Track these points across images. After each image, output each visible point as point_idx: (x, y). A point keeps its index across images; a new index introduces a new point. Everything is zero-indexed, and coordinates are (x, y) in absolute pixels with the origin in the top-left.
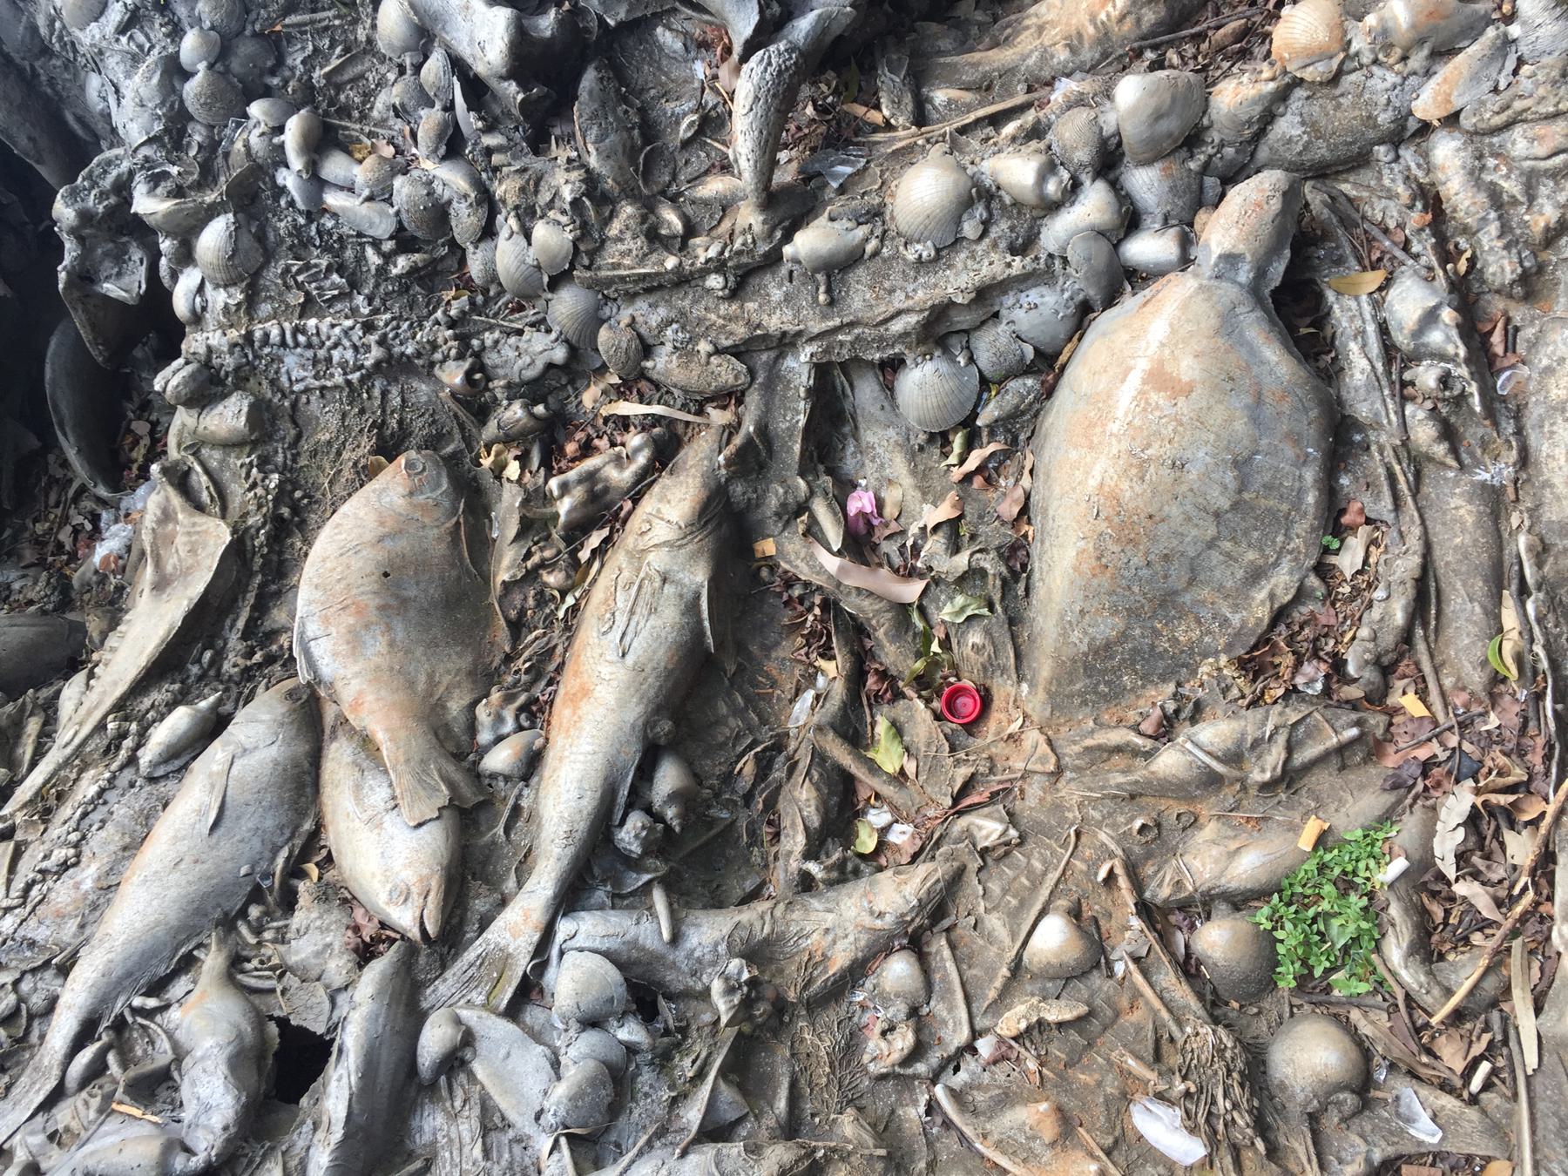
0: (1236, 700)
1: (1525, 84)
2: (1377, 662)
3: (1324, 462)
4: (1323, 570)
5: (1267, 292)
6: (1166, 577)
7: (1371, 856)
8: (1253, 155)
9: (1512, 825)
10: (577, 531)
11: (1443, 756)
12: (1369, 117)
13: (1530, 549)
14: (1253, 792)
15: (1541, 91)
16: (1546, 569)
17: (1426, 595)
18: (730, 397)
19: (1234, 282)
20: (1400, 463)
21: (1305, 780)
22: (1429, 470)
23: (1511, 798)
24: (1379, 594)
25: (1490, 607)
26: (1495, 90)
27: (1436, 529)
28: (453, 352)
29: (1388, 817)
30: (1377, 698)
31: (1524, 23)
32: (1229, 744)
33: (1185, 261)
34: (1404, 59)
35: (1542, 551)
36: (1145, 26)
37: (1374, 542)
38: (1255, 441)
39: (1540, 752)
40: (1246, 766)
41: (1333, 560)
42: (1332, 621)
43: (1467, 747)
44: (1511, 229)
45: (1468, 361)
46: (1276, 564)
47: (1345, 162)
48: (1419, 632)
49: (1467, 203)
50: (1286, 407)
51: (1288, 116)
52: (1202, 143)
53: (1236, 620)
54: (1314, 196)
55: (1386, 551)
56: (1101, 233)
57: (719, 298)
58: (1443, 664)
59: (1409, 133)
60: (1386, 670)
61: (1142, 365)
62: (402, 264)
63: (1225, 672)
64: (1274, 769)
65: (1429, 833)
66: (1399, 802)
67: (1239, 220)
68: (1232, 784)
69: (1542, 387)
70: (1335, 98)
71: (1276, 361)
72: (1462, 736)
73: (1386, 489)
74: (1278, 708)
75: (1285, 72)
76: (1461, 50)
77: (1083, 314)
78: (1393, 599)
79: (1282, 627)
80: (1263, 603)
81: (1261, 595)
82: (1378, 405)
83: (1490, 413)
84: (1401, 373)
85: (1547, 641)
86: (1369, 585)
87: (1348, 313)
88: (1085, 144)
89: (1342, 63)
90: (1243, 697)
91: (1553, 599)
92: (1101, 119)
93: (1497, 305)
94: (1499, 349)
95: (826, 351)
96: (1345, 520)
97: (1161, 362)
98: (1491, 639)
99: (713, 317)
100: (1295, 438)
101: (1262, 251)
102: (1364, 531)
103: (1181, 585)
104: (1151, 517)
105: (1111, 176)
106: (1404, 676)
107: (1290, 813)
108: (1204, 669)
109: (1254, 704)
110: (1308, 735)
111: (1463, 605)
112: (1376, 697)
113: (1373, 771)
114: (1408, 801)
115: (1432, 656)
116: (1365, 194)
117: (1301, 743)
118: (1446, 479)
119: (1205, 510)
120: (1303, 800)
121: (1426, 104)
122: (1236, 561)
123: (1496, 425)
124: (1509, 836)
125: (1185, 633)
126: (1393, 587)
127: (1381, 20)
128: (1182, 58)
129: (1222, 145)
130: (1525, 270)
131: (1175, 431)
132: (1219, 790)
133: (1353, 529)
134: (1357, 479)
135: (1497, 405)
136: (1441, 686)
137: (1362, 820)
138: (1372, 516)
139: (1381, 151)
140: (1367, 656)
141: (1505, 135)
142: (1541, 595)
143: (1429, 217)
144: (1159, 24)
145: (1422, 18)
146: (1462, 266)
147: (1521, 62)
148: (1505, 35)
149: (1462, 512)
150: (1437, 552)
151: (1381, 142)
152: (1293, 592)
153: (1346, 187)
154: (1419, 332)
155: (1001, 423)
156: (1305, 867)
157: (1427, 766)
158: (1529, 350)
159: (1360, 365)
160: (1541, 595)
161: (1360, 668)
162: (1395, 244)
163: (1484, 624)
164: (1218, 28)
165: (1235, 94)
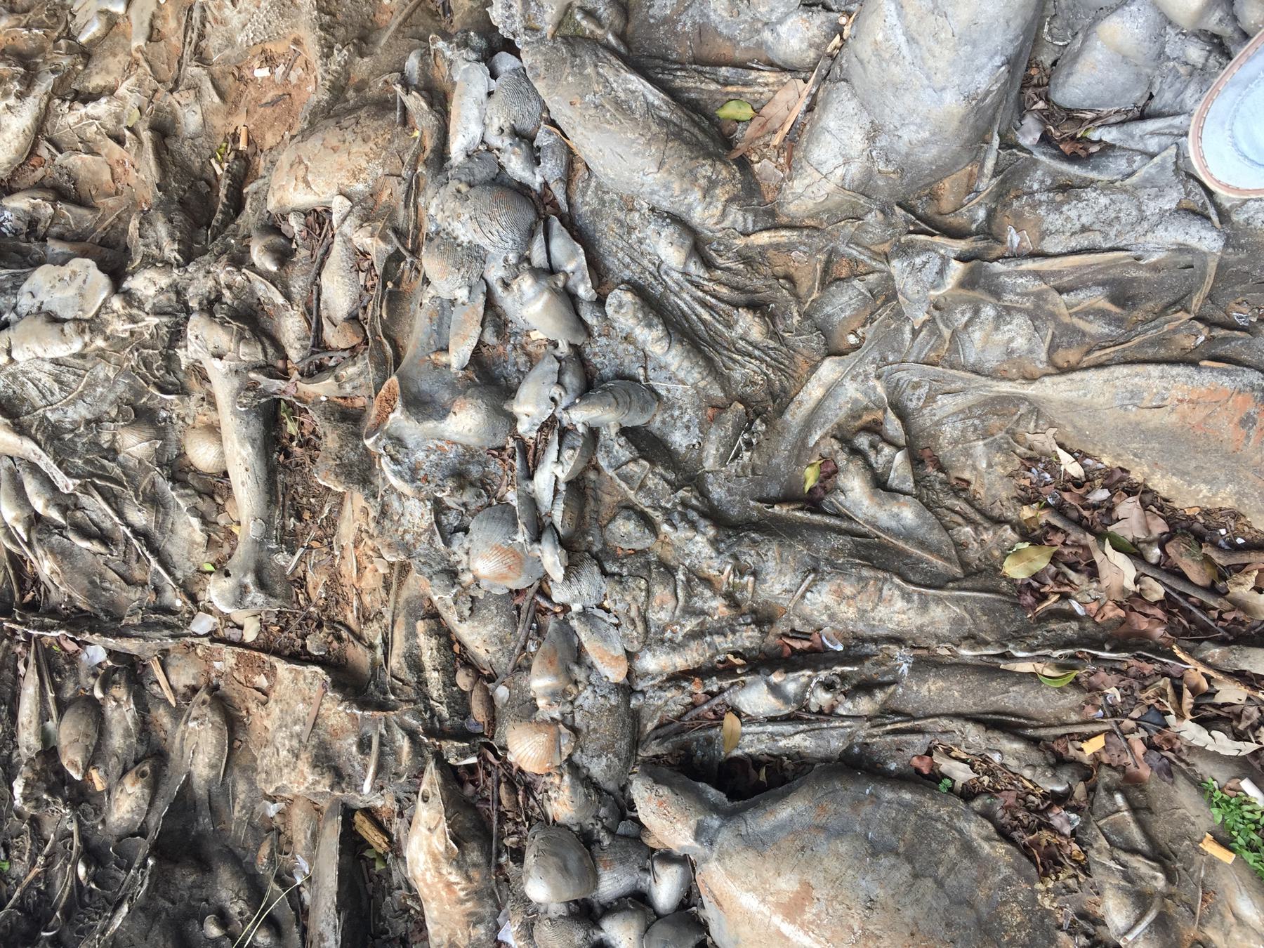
0: (1079, 883)
1: (620, 607)
2: (1054, 767)
3: (879, 782)
4: (968, 794)
5: (729, 804)
6: (965, 928)
7: (1239, 806)
8: (609, 793)
9: (1212, 694)
11: (1144, 734)
12: (610, 710)
13: (972, 648)
14: (1174, 889)
15: (628, 598)
16: (989, 639)
19: (718, 830)
20: (885, 725)
21: (1162, 842)
22: (893, 705)
23: (1187, 693)
24: (996, 758)
25: (1014, 680)
26: (617, 626)
27: (943, 707)
29: (1199, 784)
30: (1086, 772)
31: (574, 601)
32: (1128, 902)
33: (684, 861)
34: (576, 683)
35: (974, 640)
36: (481, 860)
37: (947, 752)
38: (857, 836)
39: (1144, 664)
40: (1148, 890)
41: (959, 785)
42: (1013, 794)
43: (1136, 714)
44: (722, 628)
45: (816, 670)
46: (960, 832)
47: (634, 728)
48: (1030, 732)
49: (695, 655)
50: (832, 807)
51: (591, 767)
52: (590, 833)
53: (1006, 871)
54: (653, 749)
55: (958, 746)
56: (647, 930)
58: (1059, 719)
60: (1060, 762)
61: (777, 920)
63: (1050, 886)
64: (1153, 868)
65: (1215, 757)
66: (1183, 772)
67: (665, 818)
68: (1166, 906)
69: (843, 622)
70: (588, 733)
71: (789, 810)
72: (1126, 716)
73: (904, 738)
74: (1092, 853)
75: (560, 766)
76: (580, 644)
78: (1002, 749)
79: (1015, 835)
80: (993, 847)
81: (986, 848)
82: (834, 733)
83: (859, 659)
84: (810, 712)
85: (1049, 646)
86: (985, 761)
87: (753, 742)
88: (570, 932)
89: (566, 726)
90: (1076, 877)
91: (1014, 638)
92: (553, 915)
93: (772, 640)
94: (807, 644)
96: (926, 771)
97: (778, 905)
98: (1041, 682)
100: (857, 803)
101: (699, 806)
102: (937, 758)
103: (971, 914)
104: (912, 935)
105: (599, 911)
106: (1067, 749)
107: (1198, 864)
108: (1047, 903)
109: (1086, 869)
110: (1119, 833)
111: (1011, 698)
112: (1083, 772)
113: (1153, 786)
114: (1183, 766)
115: (1051, 726)
116: (659, 714)
117: (1127, 840)
118: (904, 695)
119: (911, 886)
120: (1182, 849)
122: (955, 865)
123: (867, 656)
124: (1219, 699)
126: (991, 747)
127: (544, 696)
128: (514, 833)
129: (597, 817)
130: (753, 622)
131: (841, 903)
132: (1171, 917)
133: (933, 766)
134: (892, 757)
135: (851, 653)
136: (1078, 723)
137: (1202, 806)
138: (925, 750)
139: (634, 703)
140: (1049, 774)
141: (651, 623)
142: (1011, 645)
143: (697, 680)
144: (482, 849)
145: (552, 669)
146: (739, 661)
147: (600, 606)
148: (579, 614)
149: (933, 688)
150: (964, 710)
151: (629, 702)
152: (985, 822)
153: (650, 727)
154: (785, 698)
156: (1251, 862)
157: (1150, 746)
158: (811, 625)
159: (799, 740)
160: (1011, 645)
161: (1059, 782)
162: (707, 702)
163: (1029, 686)
164: (500, 802)
165: (563, 804)
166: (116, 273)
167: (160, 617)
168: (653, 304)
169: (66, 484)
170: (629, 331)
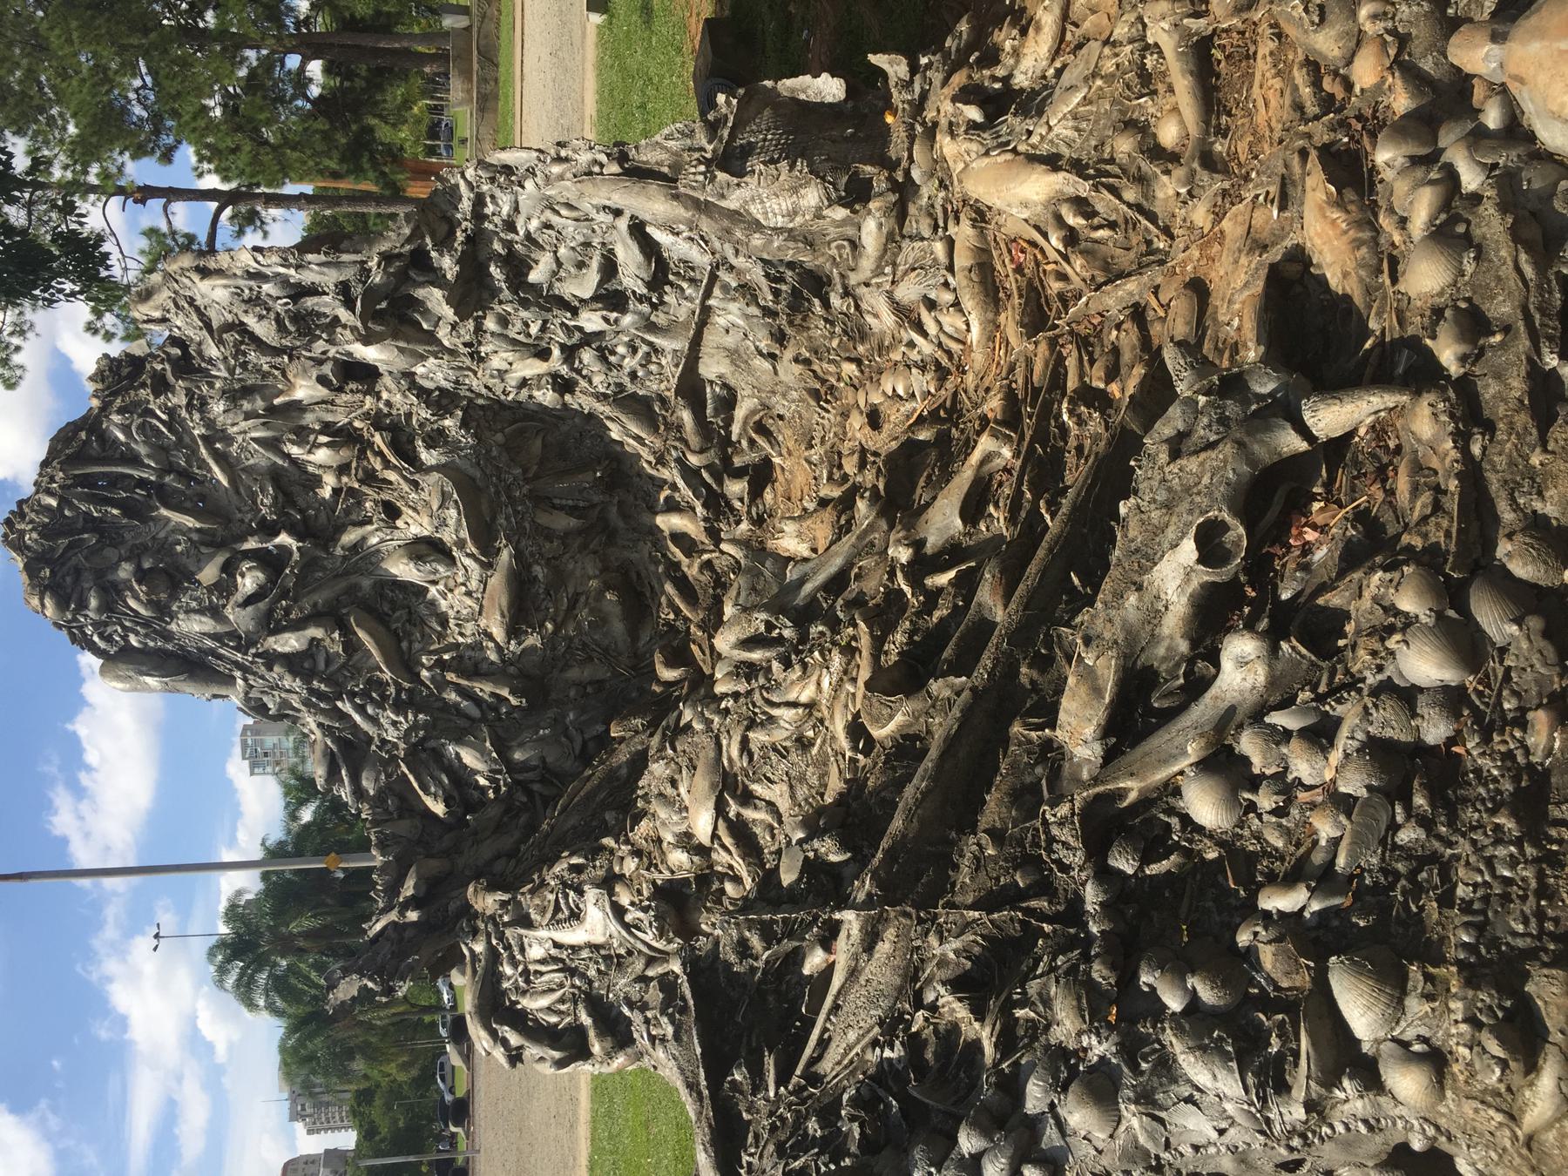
28: (1518, 734)
57: (1491, 441)
62: (1419, 800)
95: (1550, 338)
99: (1509, 445)
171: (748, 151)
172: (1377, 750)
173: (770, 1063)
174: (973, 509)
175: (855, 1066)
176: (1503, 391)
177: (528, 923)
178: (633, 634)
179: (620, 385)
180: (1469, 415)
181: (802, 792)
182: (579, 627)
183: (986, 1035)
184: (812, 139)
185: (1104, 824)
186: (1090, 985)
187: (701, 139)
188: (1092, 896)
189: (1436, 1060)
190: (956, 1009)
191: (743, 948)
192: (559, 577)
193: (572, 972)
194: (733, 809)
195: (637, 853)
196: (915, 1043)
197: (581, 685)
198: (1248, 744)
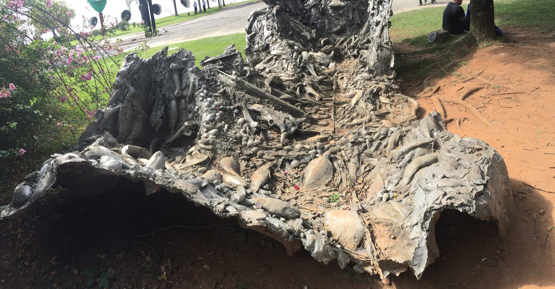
10: (252, 168)
17: (341, 181)
18: (271, 160)
59: (340, 150)
77: (311, 159)
111: (344, 181)
121: (341, 148)
125: (320, 182)
155: (302, 166)
165: (326, 146)
166: (372, 110)
167: (336, 119)
168: (380, 144)
169: (349, 109)
170: (375, 144)
171: (382, 50)
172: (241, 137)
173: (222, 67)
174: (311, 95)
175: (219, 78)
176: (280, 153)
177: (267, 20)
178: (334, 33)
179: (371, 25)
180: (278, 149)
181: (276, 69)
182: (334, 21)
183: (217, 94)
184: (383, 62)
185: (240, 108)
186: (220, 105)
187: (385, 41)
188: (232, 107)
189: (207, 137)
190: (222, 90)
191: (237, 62)
192: (341, 16)
193: (260, 30)
194: (275, 58)
195: (276, 40)
196: (219, 86)
197: (324, 23)
198: (246, 124)
